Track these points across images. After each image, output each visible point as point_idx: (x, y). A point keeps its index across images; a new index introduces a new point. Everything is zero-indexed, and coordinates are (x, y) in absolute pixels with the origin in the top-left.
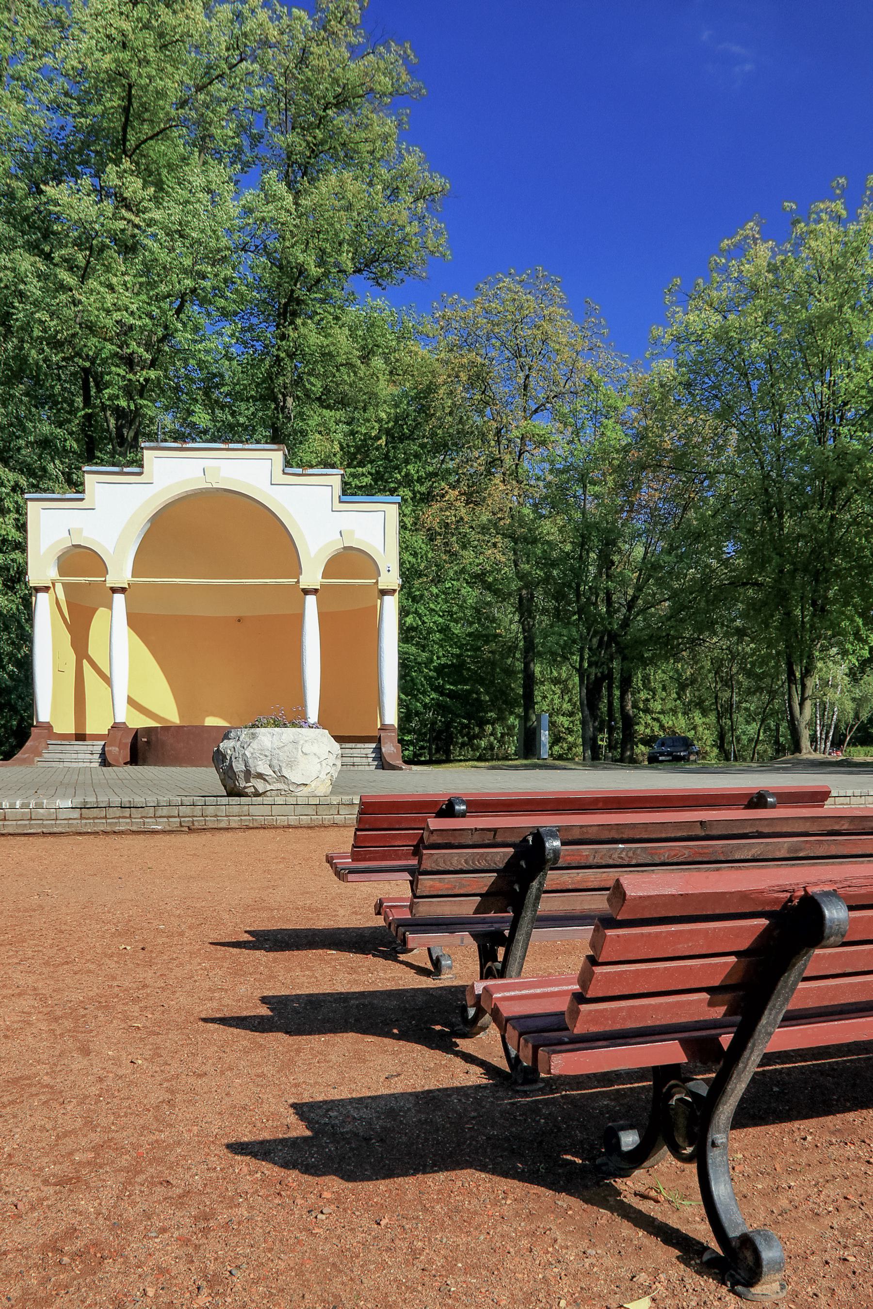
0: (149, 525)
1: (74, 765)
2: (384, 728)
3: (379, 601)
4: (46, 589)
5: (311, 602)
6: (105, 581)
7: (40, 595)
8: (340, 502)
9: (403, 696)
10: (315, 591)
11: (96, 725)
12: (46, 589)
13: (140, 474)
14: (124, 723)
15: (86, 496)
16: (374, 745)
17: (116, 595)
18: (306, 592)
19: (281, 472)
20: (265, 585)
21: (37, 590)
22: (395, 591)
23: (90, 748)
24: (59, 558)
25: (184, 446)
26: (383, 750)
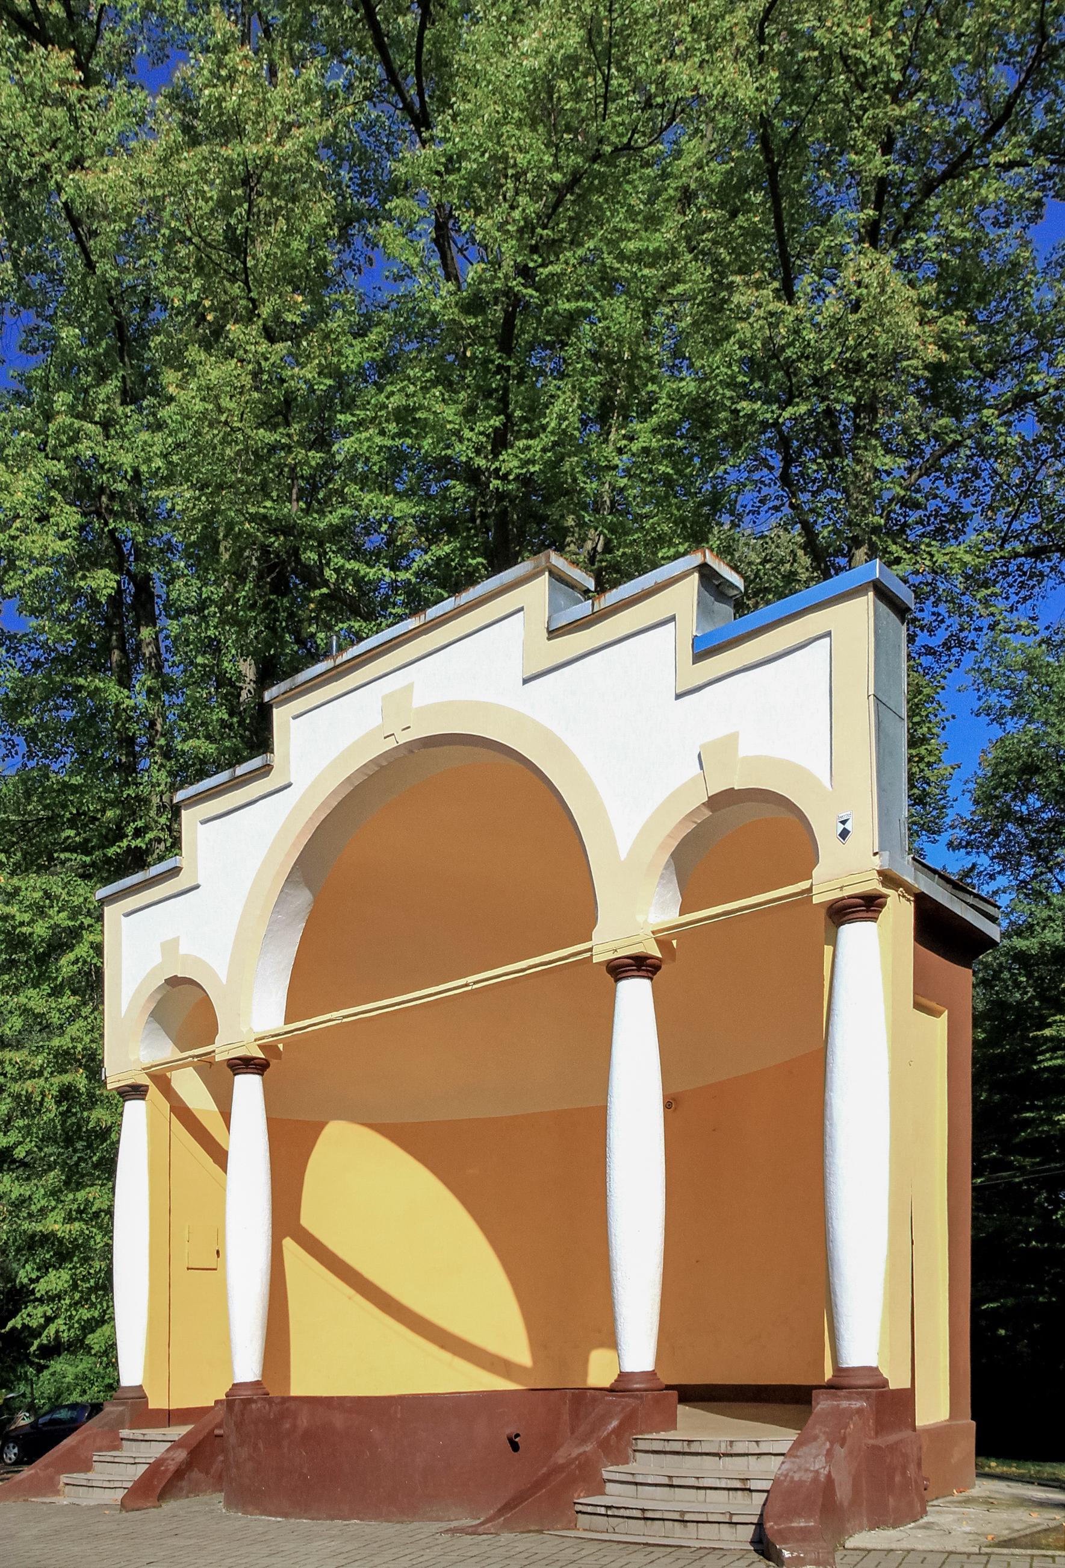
3: (828, 949)
4: (136, 1091)
12: (136, 1091)
14: (877, 1369)
17: (129, 1105)
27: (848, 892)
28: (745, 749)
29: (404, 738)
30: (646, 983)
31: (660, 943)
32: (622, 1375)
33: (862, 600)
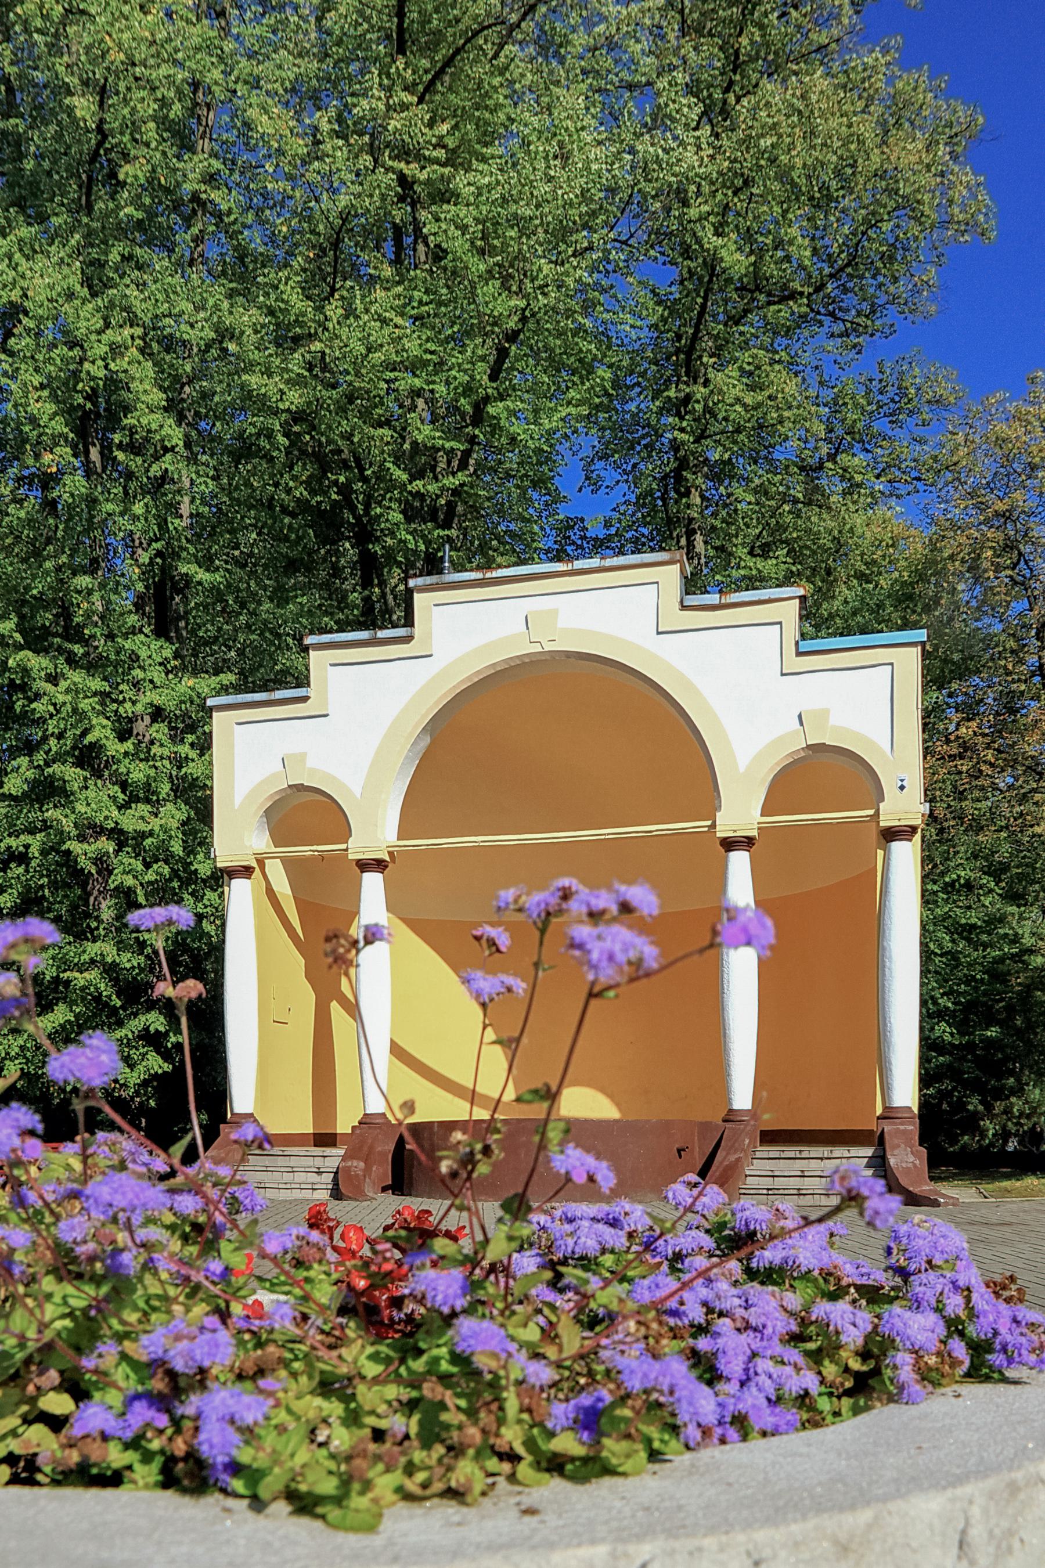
0: (428, 740)
1: (283, 1195)
2: (890, 1114)
3: (880, 853)
4: (246, 871)
5: (739, 862)
6: (346, 850)
7: (236, 883)
8: (799, 654)
9: (487, 984)
10: (748, 843)
11: (344, 1125)
12: (246, 871)
13: (408, 639)
15: (312, 691)
16: (869, 1151)
17: (366, 876)
18: (729, 844)
19: (677, 606)
20: (649, 837)
21: (232, 873)
22: (913, 829)
23: (319, 1162)
24: (268, 813)
25: (488, 575)
26: (892, 1161)
27: (903, 823)
28: (835, 720)
29: (549, 647)
30: (380, 875)
31: (391, 853)
32: (365, 1115)
33: (914, 649)
